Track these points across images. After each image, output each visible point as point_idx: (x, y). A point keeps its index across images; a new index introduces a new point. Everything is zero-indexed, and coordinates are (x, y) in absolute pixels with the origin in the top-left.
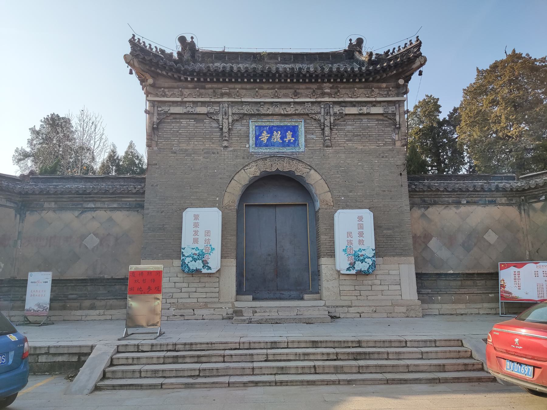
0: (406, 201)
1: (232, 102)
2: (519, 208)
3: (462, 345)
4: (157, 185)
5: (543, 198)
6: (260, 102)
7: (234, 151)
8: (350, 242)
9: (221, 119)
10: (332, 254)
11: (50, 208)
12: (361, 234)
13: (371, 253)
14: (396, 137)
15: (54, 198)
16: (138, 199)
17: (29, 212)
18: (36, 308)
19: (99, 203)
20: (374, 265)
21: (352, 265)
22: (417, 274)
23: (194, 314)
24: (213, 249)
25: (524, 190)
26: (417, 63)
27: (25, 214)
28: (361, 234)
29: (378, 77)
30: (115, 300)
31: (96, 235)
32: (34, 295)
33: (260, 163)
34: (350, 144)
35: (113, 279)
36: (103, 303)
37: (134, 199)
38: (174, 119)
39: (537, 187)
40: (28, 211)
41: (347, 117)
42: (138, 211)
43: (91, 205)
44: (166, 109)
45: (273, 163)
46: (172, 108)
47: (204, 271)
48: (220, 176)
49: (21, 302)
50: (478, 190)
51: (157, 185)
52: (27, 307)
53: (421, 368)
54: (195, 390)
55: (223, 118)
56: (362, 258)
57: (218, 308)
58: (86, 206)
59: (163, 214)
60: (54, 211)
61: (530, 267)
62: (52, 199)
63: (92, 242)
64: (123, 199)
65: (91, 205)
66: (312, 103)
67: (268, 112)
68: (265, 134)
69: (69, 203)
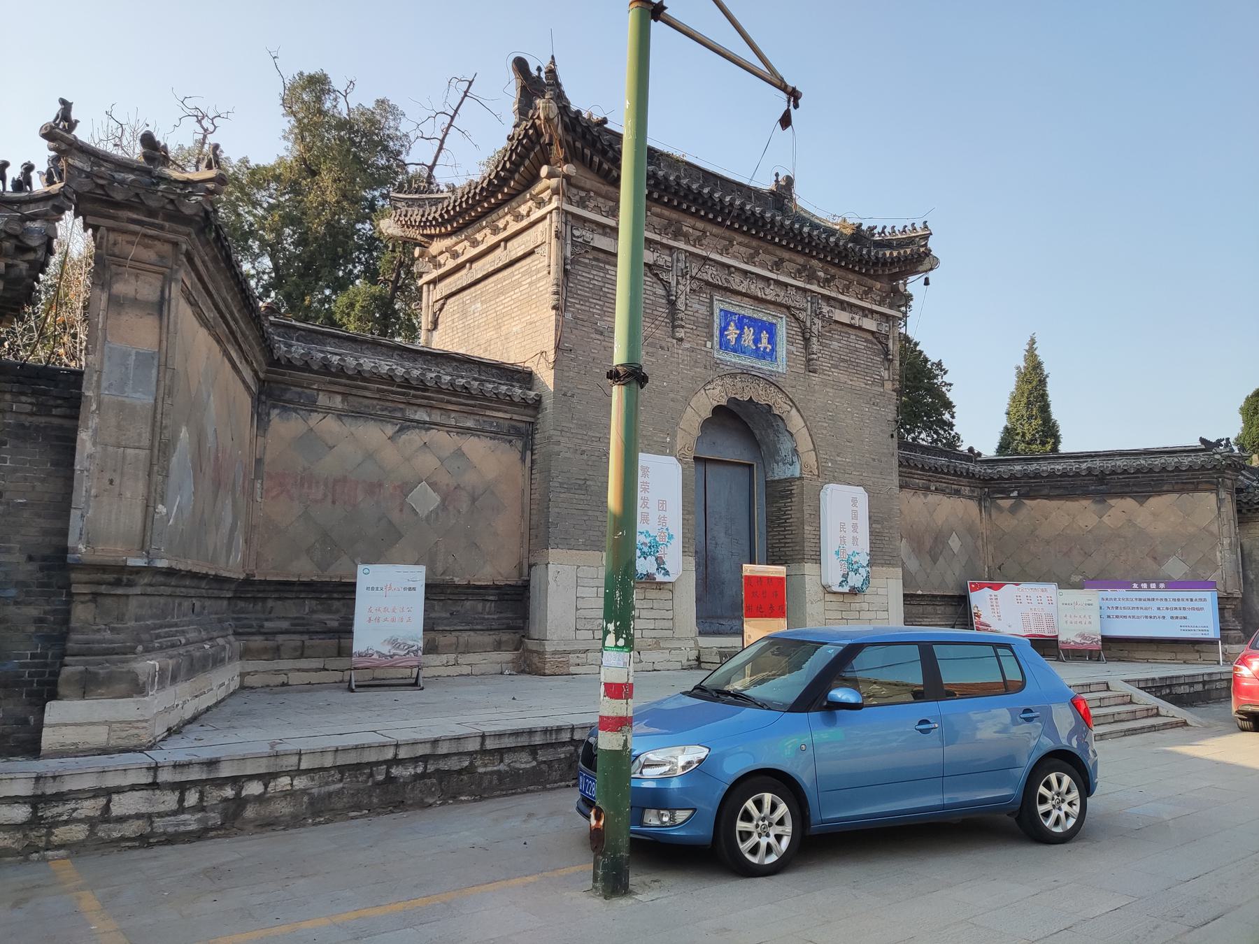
0: (896, 480)
1: (691, 254)
2: (980, 504)
3: (1108, 689)
4: (572, 396)
5: (1015, 494)
6: (729, 267)
7: (692, 350)
8: (843, 539)
9: (674, 283)
10: (817, 560)
11: (330, 408)
12: (855, 527)
13: (864, 560)
14: (885, 374)
15: (345, 385)
16: (515, 417)
17: (276, 411)
18: (386, 650)
19: (438, 412)
20: (867, 580)
21: (845, 576)
22: (905, 595)
23: (641, 661)
24: (670, 537)
25: (992, 479)
26: (926, 265)
27: (268, 414)
28: (855, 527)
29: (711, 216)
30: (472, 633)
31: (433, 485)
32: (378, 620)
33: (728, 380)
34: (836, 373)
35: (468, 586)
36: (451, 638)
37: (508, 416)
38: (596, 259)
39: (1013, 477)
40: (274, 407)
41: (833, 326)
42: (510, 442)
43: (422, 415)
44: (588, 235)
45: (744, 384)
46: (596, 237)
47: (660, 578)
48: (671, 395)
49: (261, 638)
50: (316, 368)
51: (572, 396)
52: (359, 646)
53: (1123, 716)
54: (208, 842)
55: (678, 283)
56: (855, 567)
57: (675, 649)
58: (412, 417)
59: (585, 457)
60: (339, 417)
61: (1009, 589)
62: (340, 389)
63: (425, 500)
64: (488, 413)
65: (422, 415)
66: (798, 288)
67: (740, 289)
68: (732, 327)
69: (375, 402)
